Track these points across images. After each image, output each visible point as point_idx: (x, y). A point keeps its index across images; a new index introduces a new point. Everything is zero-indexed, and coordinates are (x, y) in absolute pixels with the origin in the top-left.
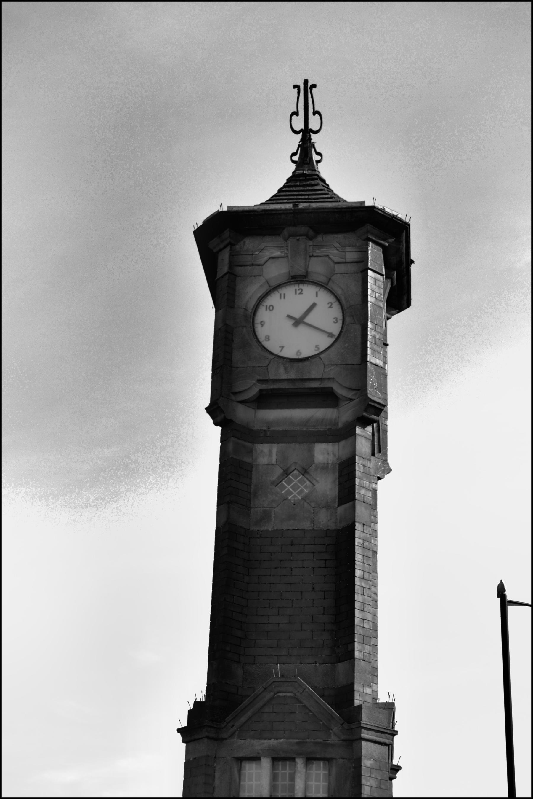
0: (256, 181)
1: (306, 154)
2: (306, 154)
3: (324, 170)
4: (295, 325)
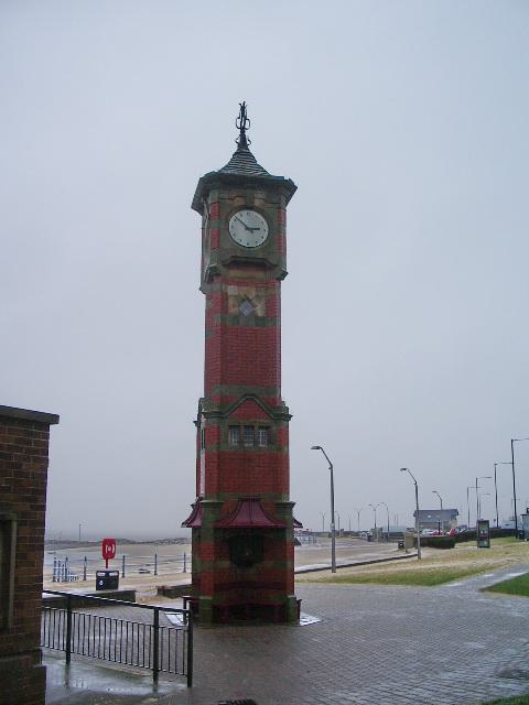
0: (219, 158)
1: (243, 142)
2: (243, 142)
3: (252, 149)
4: (246, 230)
